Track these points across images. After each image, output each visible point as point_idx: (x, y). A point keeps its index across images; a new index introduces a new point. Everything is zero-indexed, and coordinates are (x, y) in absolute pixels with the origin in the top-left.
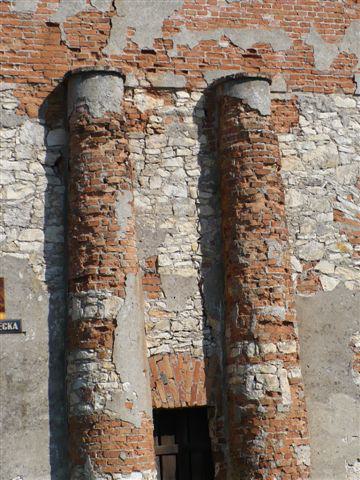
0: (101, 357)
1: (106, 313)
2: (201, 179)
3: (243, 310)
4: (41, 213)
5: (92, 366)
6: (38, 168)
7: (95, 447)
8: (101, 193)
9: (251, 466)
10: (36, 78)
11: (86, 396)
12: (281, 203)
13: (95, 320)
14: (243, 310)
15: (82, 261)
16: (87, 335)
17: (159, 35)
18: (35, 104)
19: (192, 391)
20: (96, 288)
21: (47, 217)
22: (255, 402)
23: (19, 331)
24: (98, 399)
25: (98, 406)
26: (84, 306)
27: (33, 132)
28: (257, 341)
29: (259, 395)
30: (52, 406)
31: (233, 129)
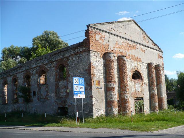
0: (114, 92)
1: (114, 86)
2: (117, 69)
3: (125, 87)
4: (103, 72)
5: (112, 94)
6: (102, 65)
7: (113, 105)
8: (113, 70)
9: (126, 108)
10: (102, 52)
11: (112, 98)
12: (8, 72)
13: (112, 87)
14: (125, 87)
15: (110, 79)
16: (111, 89)
17: (113, 48)
18: (102, 56)
19: (35, 96)
20: (112, 83)
21: (104, 72)
22: (127, 99)
23: (101, 88)
24: (113, 98)
25: (113, 99)
26: (111, 85)
27: (102, 60)
28: (126, 91)
29: (127, 98)
30: (105, 99)
31: (123, 63)
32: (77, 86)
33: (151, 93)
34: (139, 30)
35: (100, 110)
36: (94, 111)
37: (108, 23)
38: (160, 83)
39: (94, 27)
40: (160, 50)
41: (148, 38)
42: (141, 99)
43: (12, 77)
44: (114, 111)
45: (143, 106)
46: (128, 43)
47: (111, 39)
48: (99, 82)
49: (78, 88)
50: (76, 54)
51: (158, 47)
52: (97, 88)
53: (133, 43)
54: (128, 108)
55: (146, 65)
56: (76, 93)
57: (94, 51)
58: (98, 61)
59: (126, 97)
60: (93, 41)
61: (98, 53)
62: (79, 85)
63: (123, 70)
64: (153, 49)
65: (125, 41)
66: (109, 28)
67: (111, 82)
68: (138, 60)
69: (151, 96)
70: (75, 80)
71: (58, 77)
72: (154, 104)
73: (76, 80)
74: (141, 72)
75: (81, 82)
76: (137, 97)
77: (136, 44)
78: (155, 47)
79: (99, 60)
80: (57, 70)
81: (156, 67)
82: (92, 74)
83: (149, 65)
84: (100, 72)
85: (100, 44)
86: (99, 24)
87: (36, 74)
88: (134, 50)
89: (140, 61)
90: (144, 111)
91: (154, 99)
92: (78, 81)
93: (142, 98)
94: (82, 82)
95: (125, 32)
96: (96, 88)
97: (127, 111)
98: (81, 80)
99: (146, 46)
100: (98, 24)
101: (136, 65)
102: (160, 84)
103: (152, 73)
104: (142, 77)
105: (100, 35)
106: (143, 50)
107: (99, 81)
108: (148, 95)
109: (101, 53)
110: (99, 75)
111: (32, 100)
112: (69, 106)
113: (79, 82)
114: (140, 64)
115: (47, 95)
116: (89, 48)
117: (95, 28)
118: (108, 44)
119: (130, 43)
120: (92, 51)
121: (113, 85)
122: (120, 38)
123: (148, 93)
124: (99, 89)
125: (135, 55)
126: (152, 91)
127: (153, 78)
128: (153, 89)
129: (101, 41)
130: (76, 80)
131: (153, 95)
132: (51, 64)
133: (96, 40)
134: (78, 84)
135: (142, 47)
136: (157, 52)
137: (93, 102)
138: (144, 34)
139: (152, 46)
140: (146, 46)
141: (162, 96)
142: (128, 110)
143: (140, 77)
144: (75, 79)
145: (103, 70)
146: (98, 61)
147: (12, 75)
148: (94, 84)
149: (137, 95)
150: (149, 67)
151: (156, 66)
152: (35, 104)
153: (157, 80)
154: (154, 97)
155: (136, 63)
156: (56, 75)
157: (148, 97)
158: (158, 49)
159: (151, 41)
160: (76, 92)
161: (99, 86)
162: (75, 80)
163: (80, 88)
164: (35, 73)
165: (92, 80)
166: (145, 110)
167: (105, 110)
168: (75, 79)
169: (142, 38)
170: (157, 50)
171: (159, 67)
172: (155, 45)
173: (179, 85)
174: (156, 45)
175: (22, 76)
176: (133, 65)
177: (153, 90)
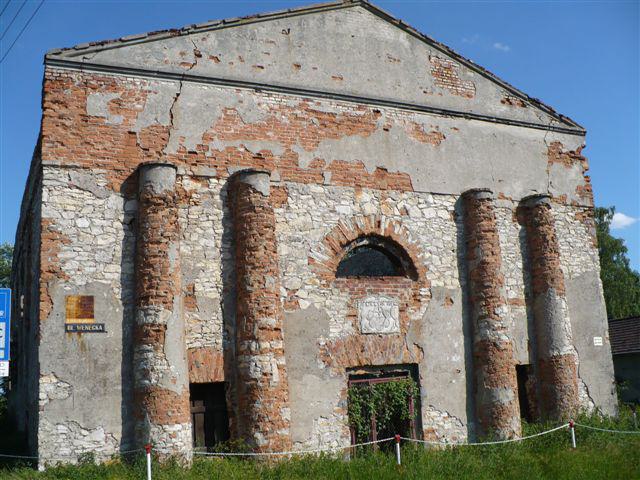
0: (156, 349)
1: (160, 320)
5: (150, 355)
6: (118, 225)
8: (159, 243)
11: (146, 374)
13: (153, 325)
15: (146, 286)
16: (147, 334)
18: (118, 183)
19: (215, 372)
21: (124, 257)
22: (255, 380)
23: (103, 331)
25: (154, 381)
26: (146, 315)
27: (116, 201)
28: (257, 340)
29: (258, 375)
33: (478, 339)
34: (407, 44)
35: (84, 432)
36: (41, 436)
37: (172, 31)
38: (546, 288)
39: (80, 59)
40: (563, 126)
41: (471, 74)
42: (405, 374)
44: (155, 438)
45: (419, 406)
46: (316, 108)
48: (86, 305)
51: (551, 112)
52: (70, 328)
53: (355, 105)
54: (261, 424)
55: (450, 203)
57: (66, 167)
59: (252, 368)
60: (63, 125)
61: (96, 170)
63: (245, 238)
64: (507, 122)
65: (295, 100)
66: (182, 54)
67: (146, 298)
68: (383, 183)
69: (479, 355)
72: (489, 392)
74: (406, 242)
76: (364, 362)
77: (372, 108)
78: (532, 114)
79: (101, 202)
81: (528, 208)
82: (44, 266)
83: (470, 209)
85: (110, 131)
86: (105, 46)
88: (354, 141)
89: (403, 184)
90: (420, 433)
91: (489, 372)
93: (412, 370)
95: (298, 60)
96: (67, 331)
97: (259, 436)
99: (445, 113)
100: (102, 44)
101: (370, 209)
102: (545, 291)
103: (481, 238)
104: (417, 265)
105: (116, 90)
106: (428, 130)
107: (91, 299)
108: (455, 351)
109: (118, 170)
110: (92, 269)
114: (404, 200)
117: (81, 66)
118: (167, 123)
119: (328, 106)
121: (156, 315)
122: (561, 116)
123: (459, 342)
124: (88, 336)
125: (366, 160)
126: (479, 328)
127: (484, 262)
128: (484, 317)
129: (117, 119)
131: (486, 350)
133: (85, 118)
135: (418, 117)
136: (540, 134)
137: (42, 395)
138: (441, 55)
139: (502, 110)
140: (445, 113)
141: (556, 353)
142: (265, 433)
143: (406, 264)
145: (119, 248)
148: (54, 313)
149: (367, 354)
150: (466, 214)
153: (533, 271)
154: (487, 361)
157: (459, 359)
158: (546, 119)
159: (492, 88)
165: (43, 296)
166: (425, 427)
167: (120, 428)
169: (427, 77)
170: (541, 127)
171: (538, 206)
172: (524, 106)
174: (536, 103)
176: (345, 208)
177: (482, 325)
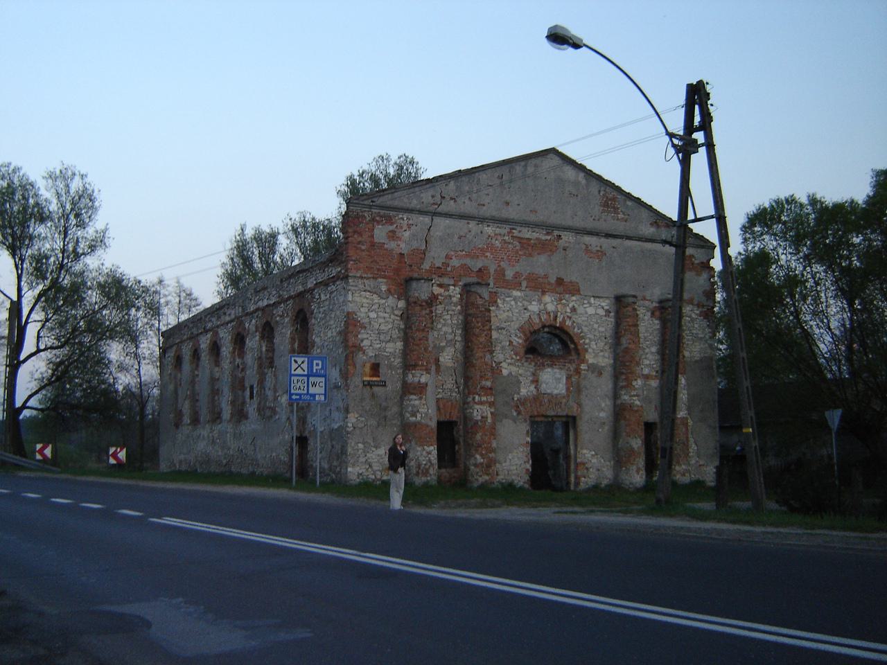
12: (201, 318)
32: (301, 378)
33: (619, 402)
34: (584, 182)
43: (209, 335)
46: (520, 235)
47: (437, 233)
49: (306, 385)
50: (325, 284)
56: (298, 397)
58: (376, 307)
62: (308, 376)
66: (433, 197)
70: (296, 362)
71: (296, 345)
73: (299, 363)
75: (315, 368)
77: (556, 233)
80: (293, 325)
84: (382, 337)
87: (256, 331)
92: (305, 366)
94: (320, 367)
98: (315, 362)
101: (550, 307)
111: (247, 412)
112: (310, 432)
113: (310, 366)
114: (573, 301)
115: (464, 404)
116: (175, 327)
118: (424, 247)
120: (355, 277)
124: (376, 389)
130: (299, 363)
132: (282, 305)
134: (306, 373)
144: (296, 359)
146: (376, 307)
147: (210, 330)
151: (663, 305)
152: (253, 426)
155: (547, 298)
156: (293, 339)
160: (297, 394)
161: (375, 379)
162: (296, 362)
163: (310, 385)
164: (254, 329)
168: (296, 359)
173: (791, 377)
175: (230, 337)
176: (534, 307)
